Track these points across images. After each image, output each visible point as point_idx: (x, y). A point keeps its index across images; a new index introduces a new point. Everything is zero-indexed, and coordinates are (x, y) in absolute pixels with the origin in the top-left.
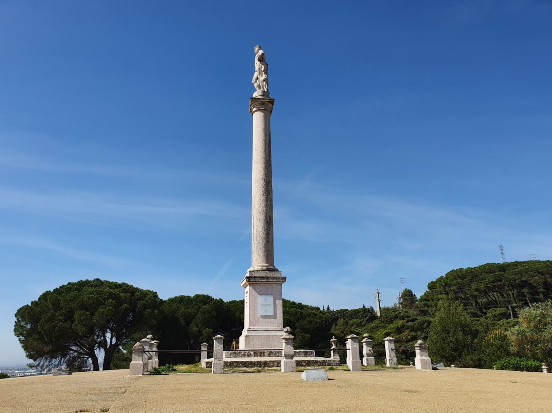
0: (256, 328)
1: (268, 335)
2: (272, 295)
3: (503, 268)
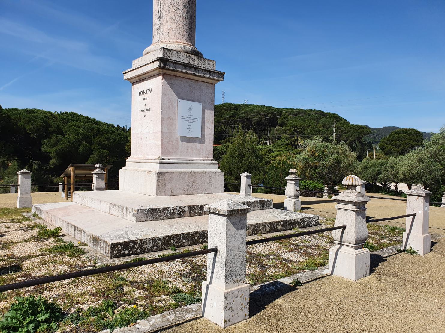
0: (174, 158)
1: (195, 173)
2: (199, 101)
3: (236, 107)
